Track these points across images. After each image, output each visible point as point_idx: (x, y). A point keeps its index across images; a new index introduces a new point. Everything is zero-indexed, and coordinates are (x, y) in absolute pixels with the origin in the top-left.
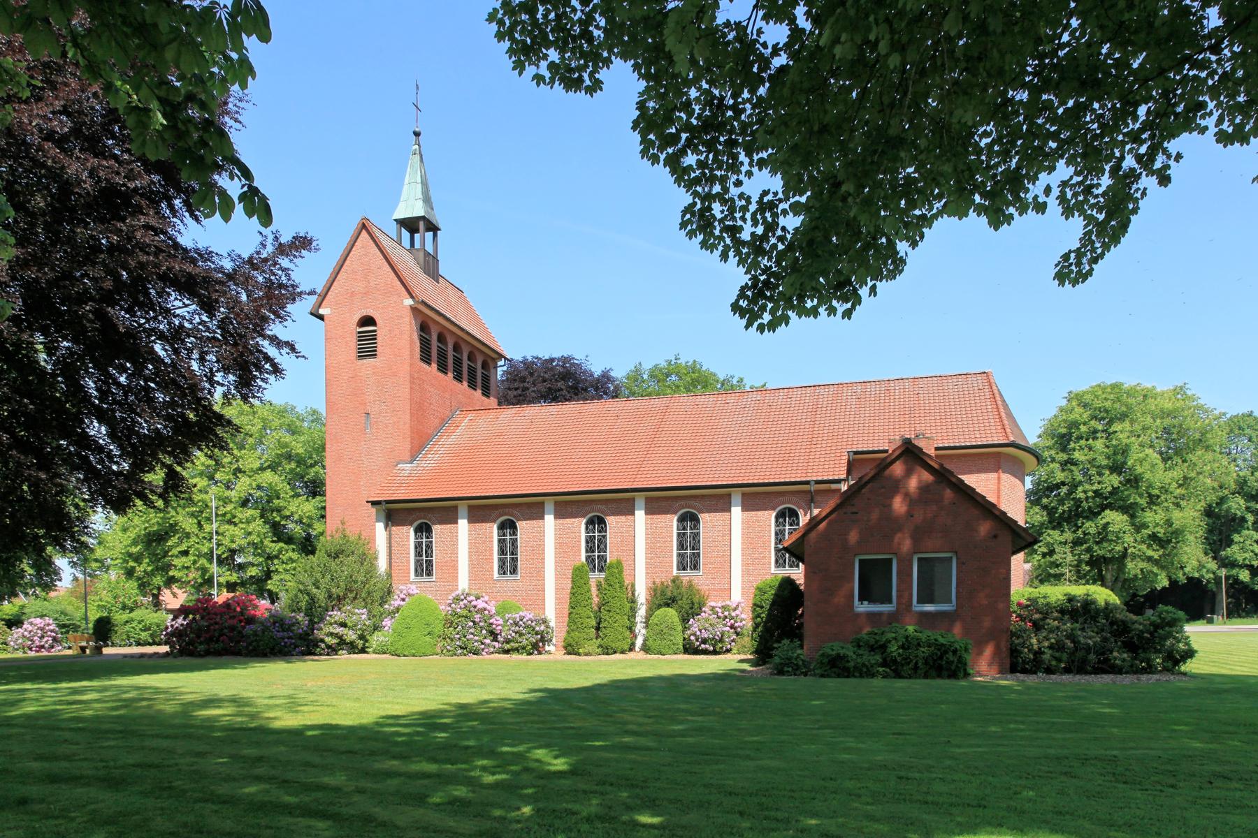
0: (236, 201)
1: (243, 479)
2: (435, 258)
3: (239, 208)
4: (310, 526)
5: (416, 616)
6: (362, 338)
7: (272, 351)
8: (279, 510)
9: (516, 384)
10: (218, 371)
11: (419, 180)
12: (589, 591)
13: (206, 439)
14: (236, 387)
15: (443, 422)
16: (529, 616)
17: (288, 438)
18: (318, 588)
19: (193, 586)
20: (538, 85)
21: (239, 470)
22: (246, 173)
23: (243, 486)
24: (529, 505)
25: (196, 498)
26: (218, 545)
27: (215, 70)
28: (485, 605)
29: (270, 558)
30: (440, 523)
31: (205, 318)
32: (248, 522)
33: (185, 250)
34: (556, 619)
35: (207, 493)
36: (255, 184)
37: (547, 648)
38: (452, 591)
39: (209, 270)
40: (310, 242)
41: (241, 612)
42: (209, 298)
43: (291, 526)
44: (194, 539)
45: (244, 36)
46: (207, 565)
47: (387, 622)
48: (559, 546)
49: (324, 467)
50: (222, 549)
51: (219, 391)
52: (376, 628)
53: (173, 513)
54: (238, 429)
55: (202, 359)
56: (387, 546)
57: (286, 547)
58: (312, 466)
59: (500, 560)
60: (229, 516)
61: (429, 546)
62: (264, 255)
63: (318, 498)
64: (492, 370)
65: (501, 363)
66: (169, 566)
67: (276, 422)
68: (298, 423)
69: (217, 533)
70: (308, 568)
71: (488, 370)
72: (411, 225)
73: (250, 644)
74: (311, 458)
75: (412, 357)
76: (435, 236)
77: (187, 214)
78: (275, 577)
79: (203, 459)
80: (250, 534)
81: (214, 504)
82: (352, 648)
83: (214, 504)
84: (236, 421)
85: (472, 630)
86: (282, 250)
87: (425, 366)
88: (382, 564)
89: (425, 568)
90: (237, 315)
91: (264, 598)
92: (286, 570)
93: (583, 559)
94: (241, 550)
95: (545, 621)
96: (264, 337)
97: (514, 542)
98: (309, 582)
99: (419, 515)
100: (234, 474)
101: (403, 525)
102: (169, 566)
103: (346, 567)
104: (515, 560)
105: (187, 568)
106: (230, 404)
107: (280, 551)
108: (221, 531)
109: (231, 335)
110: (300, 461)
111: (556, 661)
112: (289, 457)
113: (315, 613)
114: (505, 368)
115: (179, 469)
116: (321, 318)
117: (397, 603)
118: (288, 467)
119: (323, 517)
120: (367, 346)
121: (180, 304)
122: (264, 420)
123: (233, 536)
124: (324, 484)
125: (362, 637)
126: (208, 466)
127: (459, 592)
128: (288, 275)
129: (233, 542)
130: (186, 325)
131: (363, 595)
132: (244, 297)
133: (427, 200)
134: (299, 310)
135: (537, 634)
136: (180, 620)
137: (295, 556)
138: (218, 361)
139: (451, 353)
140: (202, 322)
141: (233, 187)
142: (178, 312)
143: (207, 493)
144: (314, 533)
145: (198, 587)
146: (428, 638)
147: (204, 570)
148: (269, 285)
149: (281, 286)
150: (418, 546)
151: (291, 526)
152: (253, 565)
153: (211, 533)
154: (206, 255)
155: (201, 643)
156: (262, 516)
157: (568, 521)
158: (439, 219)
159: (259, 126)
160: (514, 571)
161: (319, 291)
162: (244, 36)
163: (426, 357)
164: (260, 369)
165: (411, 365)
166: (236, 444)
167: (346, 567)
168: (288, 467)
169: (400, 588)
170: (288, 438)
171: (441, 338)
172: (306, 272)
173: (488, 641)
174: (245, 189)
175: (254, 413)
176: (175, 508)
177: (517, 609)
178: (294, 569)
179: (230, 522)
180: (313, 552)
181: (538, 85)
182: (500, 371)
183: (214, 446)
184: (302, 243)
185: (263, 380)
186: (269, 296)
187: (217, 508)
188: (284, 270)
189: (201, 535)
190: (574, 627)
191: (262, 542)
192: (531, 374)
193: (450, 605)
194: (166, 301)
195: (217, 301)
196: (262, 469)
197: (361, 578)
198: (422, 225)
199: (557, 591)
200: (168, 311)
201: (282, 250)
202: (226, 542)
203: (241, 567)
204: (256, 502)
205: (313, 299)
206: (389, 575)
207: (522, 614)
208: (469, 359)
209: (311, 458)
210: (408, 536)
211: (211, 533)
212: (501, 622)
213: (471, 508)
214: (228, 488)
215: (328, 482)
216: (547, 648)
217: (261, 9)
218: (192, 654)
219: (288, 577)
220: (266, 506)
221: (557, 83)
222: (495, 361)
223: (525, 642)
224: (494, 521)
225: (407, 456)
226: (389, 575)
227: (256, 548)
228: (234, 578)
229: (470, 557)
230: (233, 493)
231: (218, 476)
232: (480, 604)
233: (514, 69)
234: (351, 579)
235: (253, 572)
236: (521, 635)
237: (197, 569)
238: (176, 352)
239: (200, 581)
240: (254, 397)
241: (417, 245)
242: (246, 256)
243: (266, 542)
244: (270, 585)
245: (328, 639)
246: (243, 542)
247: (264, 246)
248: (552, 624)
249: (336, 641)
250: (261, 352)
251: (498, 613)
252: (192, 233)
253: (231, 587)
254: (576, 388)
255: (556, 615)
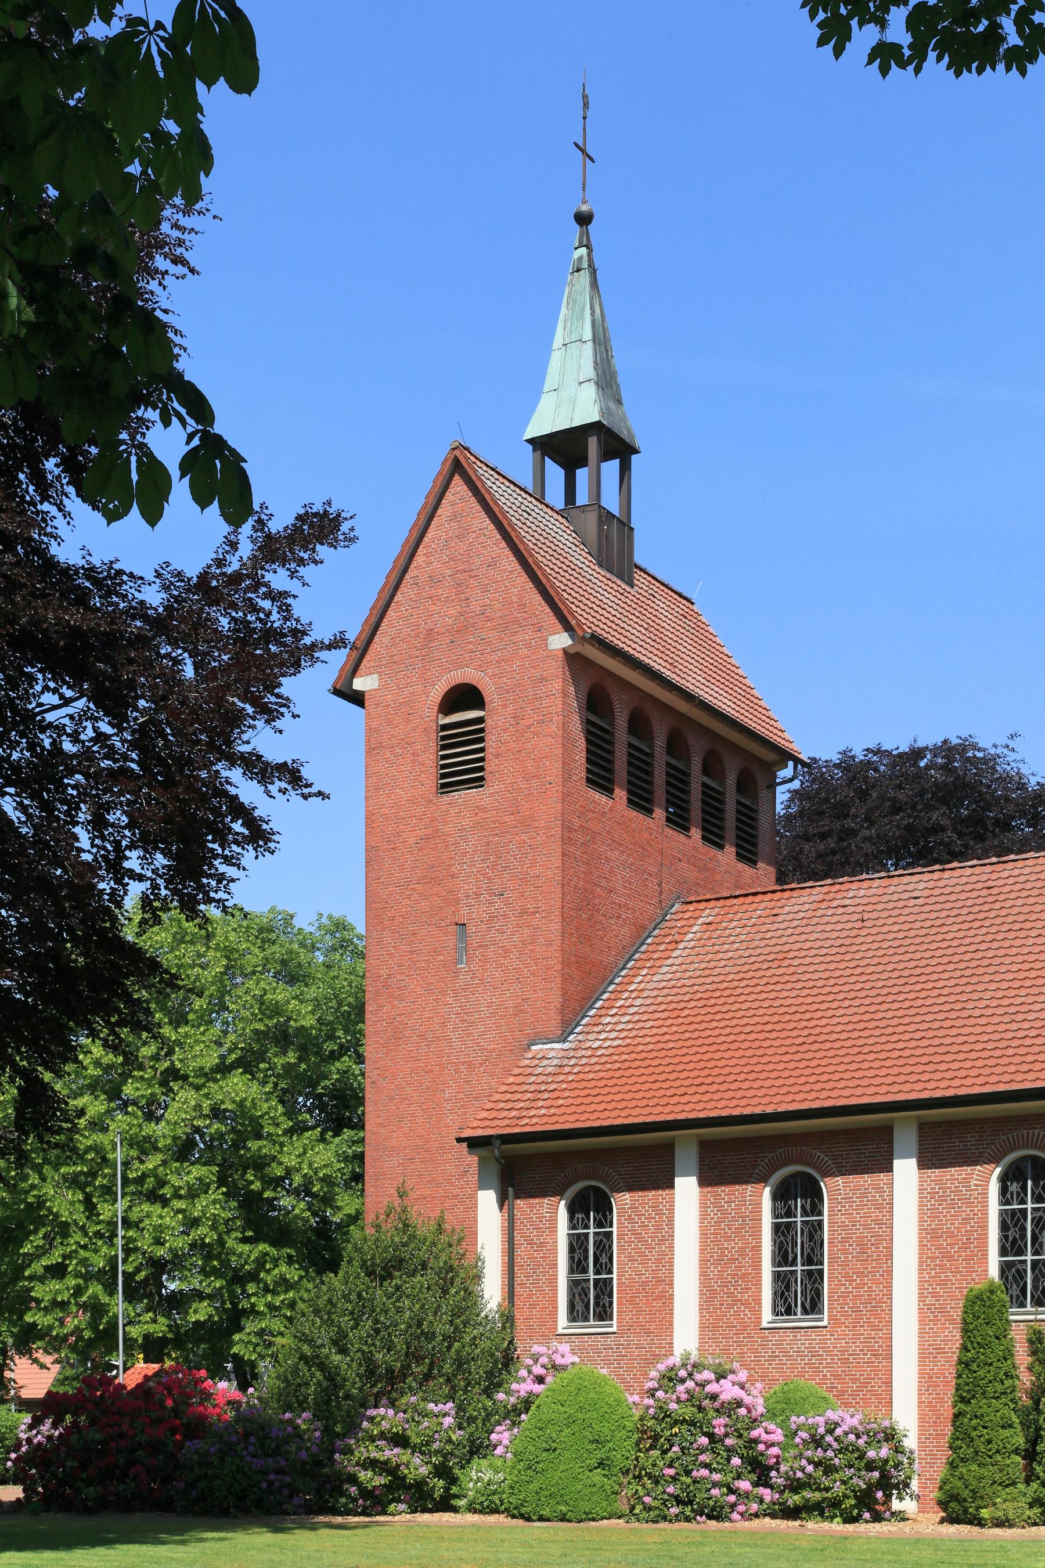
0: (174, 472)
1: (182, 1095)
2: (625, 526)
3: (181, 490)
4: (328, 1200)
5: (571, 1421)
6: (451, 739)
7: (246, 790)
8: (260, 1164)
9: (825, 824)
10: (132, 847)
11: (588, 334)
12: (1008, 1355)
13: (105, 1009)
14: (168, 882)
15: (640, 934)
16: (850, 1420)
17: (281, 993)
18: (343, 1351)
19: (73, 1348)
20: (884, 71)
21: (173, 1074)
22: (199, 407)
23: (183, 1106)
24: (853, 1135)
25: (83, 1142)
26: (128, 1251)
27: (134, 168)
28: (737, 1393)
29: (239, 1278)
30: (630, 1189)
31: (105, 728)
32: (193, 1194)
33: (67, 572)
34: (922, 1429)
35: (105, 1130)
36: (218, 428)
37: (896, 1505)
38: (657, 1358)
39: (113, 618)
40: (336, 521)
41: (175, 1410)
42: (115, 680)
43: (286, 1202)
44: (77, 1237)
45: (200, 86)
46: (105, 1299)
47: (502, 1435)
48: (930, 1236)
49: (360, 1059)
50: (136, 1259)
51: (136, 889)
52: (477, 1449)
53: (34, 1179)
54: (172, 982)
55: (98, 824)
56: (501, 1246)
57: (273, 1252)
58: (334, 1056)
59: (777, 1277)
60: (150, 1182)
61: (604, 1244)
62: (234, 566)
63: (347, 1133)
64: (763, 794)
65: (787, 772)
66: (25, 1301)
67: (254, 958)
68: (303, 957)
69: (127, 1223)
70: (321, 1303)
71: (755, 797)
72: (564, 448)
73: (193, 1485)
74: (331, 1037)
75: (567, 775)
76: (625, 469)
77: (71, 490)
78: (250, 1326)
79: (97, 1050)
80: (195, 1222)
81: (119, 1156)
82: (422, 1499)
83: (119, 1156)
84: (168, 960)
85: (705, 1458)
86: (274, 549)
87: (598, 797)
88: (492, 1292)
89: (592, 1300)
90: (174, 713)
91: (225, 1376)
92: (271, 1307)
93: (994, 1272)
94: (175, 1263)
95: (890, 1436)
96: (233, 759)
97: (814, 1230)
98: (324, 1336)
99: (581, 1169)
100: (164, 1083)
101: (544, 1195)
102: (25, 1301)
103: (410, 1300)
104: (815, 1278)
105: (63, 1305)
106: (157, 921)
107: (261, 1262)
108: (134, 1216)
109: (162, 762)
110: (306, 1044)
111: (918, 1541)
112: (283, 1038)
113: (340, 1413)
114: (796, 785)
115: (47, 1076)
116: (357, 699)
117: (525, 1387)
118: (279, 1061)
119: (358, 1178)
120: (461, 758)
121: (55, 700)
122: (229, 952)
123: (160, 1229)
124: (361, 1101)
125: (442, 1471)
126: (108, 1068)
127: (676, 1359)
128: (286, 611)
129: (159, 1242)
130: (68, 746)
131: (448, 1368)
132: (189, 671)
133: (606, 381)
134: (306, 688)
135: (870, 1466)
136: (46, 1427)
137: (293, 1274)
138: (130, 826)
139: (660, 759)
140: (100, 737)
141: (168, 442)
142: (50, 717)
143: (105, 1130)
144: (336, 1219)
145: (83, 1349)
146: (597, 1477)
147: (97, 1309)
148: (243, 630)
149: (271, 635)
150: (577, 1245)
151: (286, 1202)
152: (199, 1295)
153: (112, 1224)
154: (109, 580)
155: (89, 1482)
156: (222, 1181)
157: (956, 1173)
158: (637, 426)
159: (227, 300)
160: (813, 1306)
161: (351, 636)
162: (200, 86)
163: (600, 778)
164: (222, 835)
165: (565, 797)
166: (167, 1012)
167: (410, 1300)
168: (279, 1061)
169: (534, 1351)
170: (281, 993)
171: (638, 725)
172: (326, 597)
173: (744, 1485)
174: (196, 442)
175: (209, 936)
176: (38, 1169)
177: (821, 1404)
178: (292, 1305)
179: (154, 1197)
180: (334, 1266)
181: (884, 71)
182: (782, 795)
183: (122, 1023)
184: (320, 528)
185: (228, 860)
186: (242, 663)
187: (126, 1164)
188: (274, 596)
189: (92, 1229)
190: (967, 1451)
191: (221, 1242)
192: (863, 795)
193: (652, 1393)
194: (26, 698)
195: (132, 685)
196: (223, 1069)
197: (442, 1328)
198: (593, 444)
199: (923, 1357)
200: (30, 716)
201: (274, 549)
202: (144, 1243)
203: (178, 1302)
204: (209, 1147)
205: (338, 658)
206: (508, 1319)
207: (832, 1415)
208: (706, 771)
209: (331, 1037)
210: (554, 1221)
211: (112, 1224)
212: (778, 1436)
213: (925, 1129)
214: (150, 1116)
215: (370, 1095)
216: (896, 1505)
217: (238, 17)
218: (68, 1506)
219: (277, 1325)
220: (231, 1152)
221: (932, 55)
222: (770, 770)
223: (839, 1489)
224: (764, 1180)
225: (553, 1023)
226: (508, 1319)
227: (208, 1258)
228: (160, 1327)
229: (703, 1274)
230: (159, 1130)
231: (129, 1090)
232: (728, 1391)
233: (822, 42)
234: (418, 1327)
235: (201, 1312)
236: (829, 1469)
237: (84, 1306)
238: (47, 807)
239: (87, 1334)
240: (209, 900)
241: (582, 497)
242: (192, 572)
243: (230, 1243)
244: (241, 1345)
245: (365, 1476)
246: (181, 1243)
247: (234, 545)
248: (911, 1442)
249: (380, 1480)
250: (225, 794)
251: (771, 1414)
252: (80, 534)
253: (153, 1348)
254: (981, 822)
255: (922, 1418)
